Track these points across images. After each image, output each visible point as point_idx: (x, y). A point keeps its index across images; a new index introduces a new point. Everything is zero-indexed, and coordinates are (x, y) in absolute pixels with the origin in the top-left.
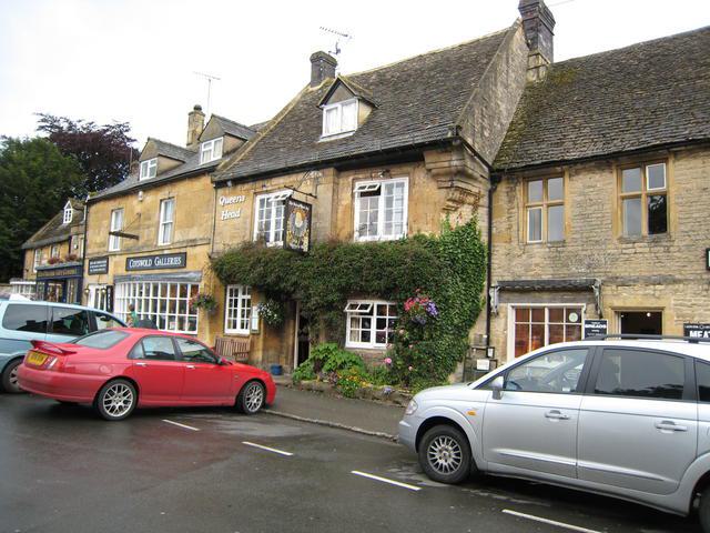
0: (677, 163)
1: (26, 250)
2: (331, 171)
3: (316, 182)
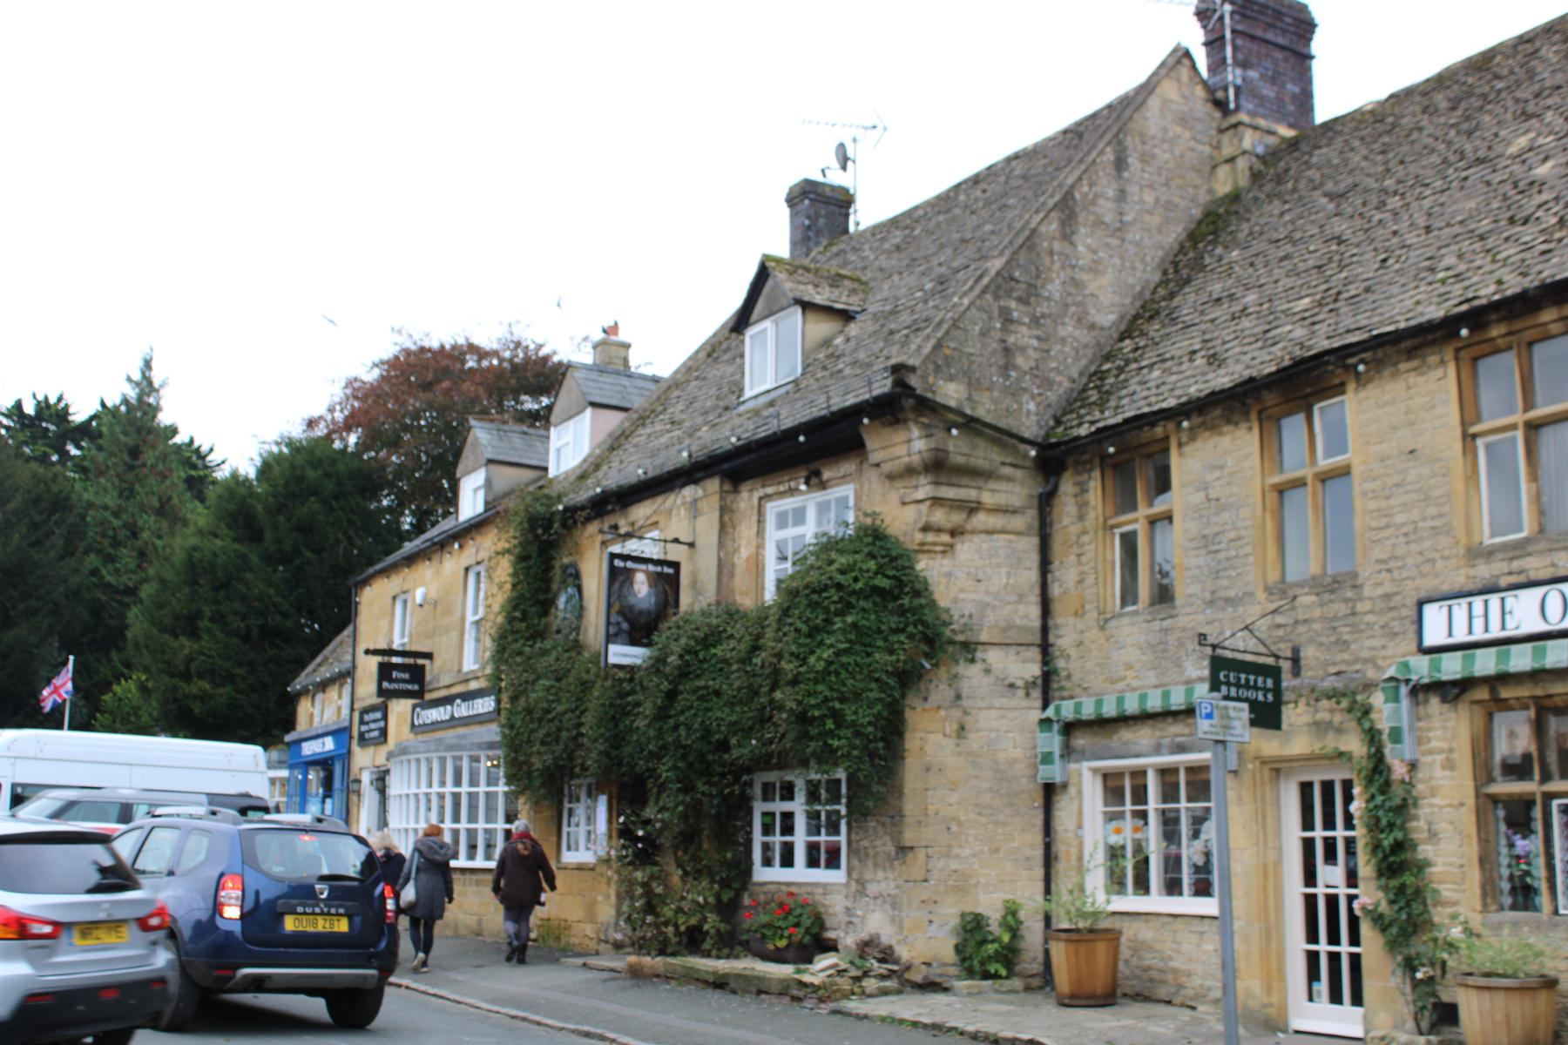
0: (1362, 394)
1: (297, 696)
2: (713, 484)
3: (694, 508)
